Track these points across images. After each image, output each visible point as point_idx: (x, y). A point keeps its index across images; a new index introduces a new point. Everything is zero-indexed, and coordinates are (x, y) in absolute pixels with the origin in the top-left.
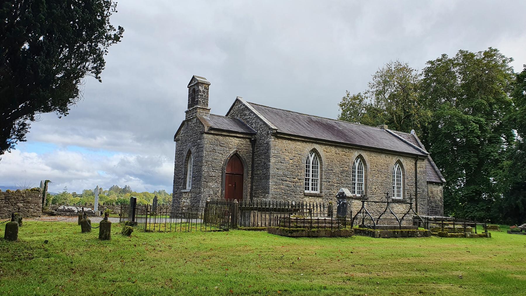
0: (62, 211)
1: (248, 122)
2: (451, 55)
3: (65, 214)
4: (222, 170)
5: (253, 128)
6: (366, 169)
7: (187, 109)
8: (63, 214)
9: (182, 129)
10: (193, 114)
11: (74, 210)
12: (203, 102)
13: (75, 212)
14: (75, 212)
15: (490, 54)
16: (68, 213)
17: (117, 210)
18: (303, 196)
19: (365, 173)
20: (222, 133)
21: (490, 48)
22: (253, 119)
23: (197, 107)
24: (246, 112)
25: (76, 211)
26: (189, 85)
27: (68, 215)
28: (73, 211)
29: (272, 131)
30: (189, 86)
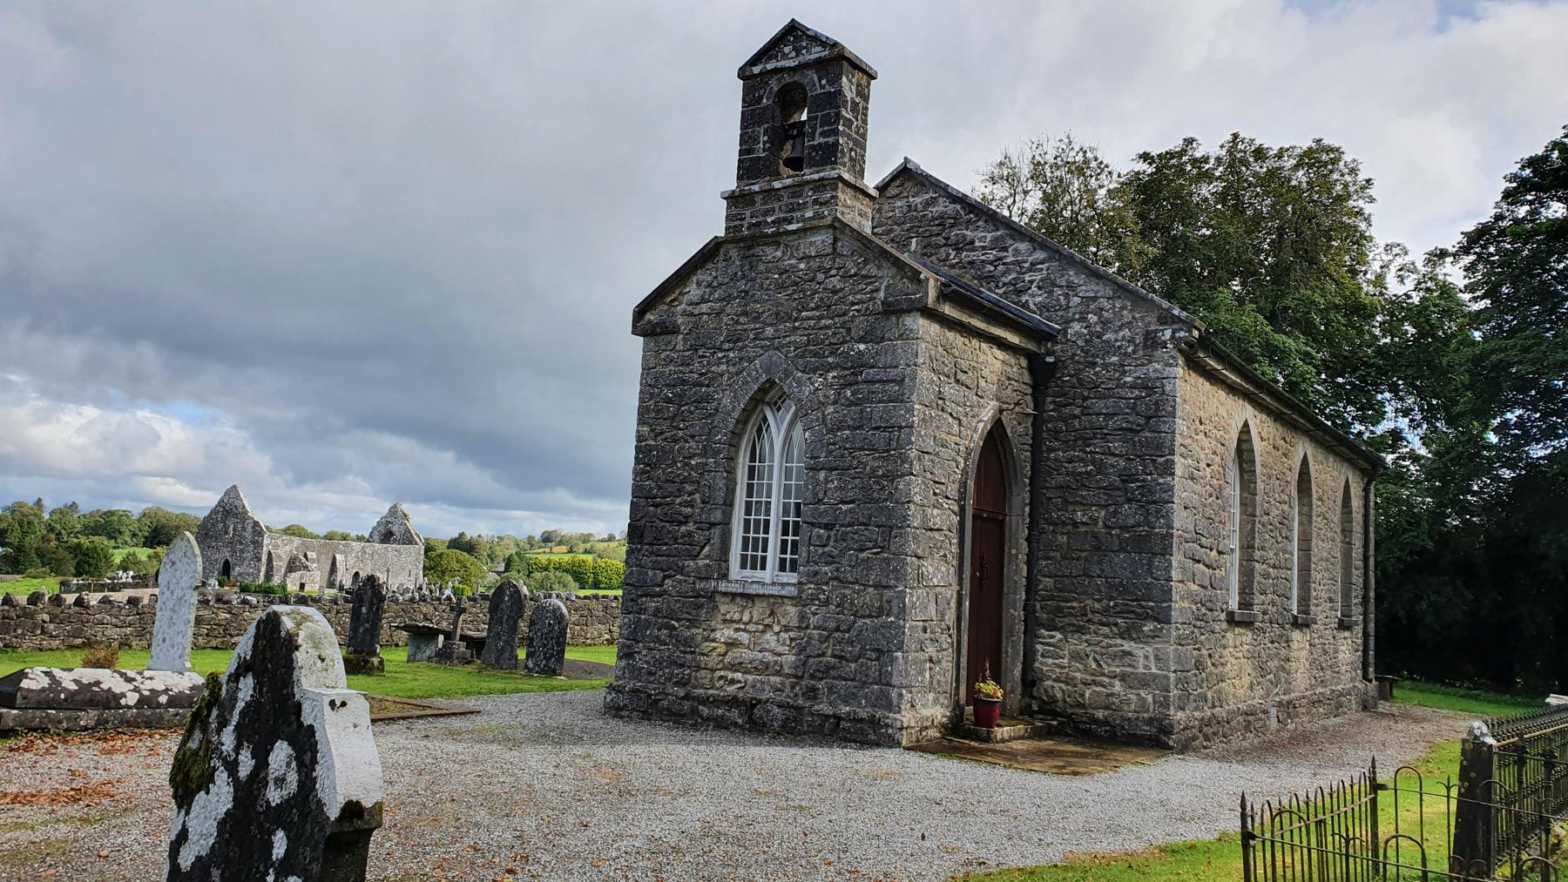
0: (49, 699)
1: (990, 278)
2: (1211, 146)
3: (68, 719)
4: (960, 500)
5: (1028, 309)
6: (1306, 509)
7: (732, 184)
8: (60, 722)
9: (701, 276)
10: (791, 211)
11: (117, 691)
12: (851, 159)
13: (123, 702)
14: (129, 707)
15: (1319, 158)
16: (87, 717)
17: (99, 628)
18: (1224, 625)
19: (1300, 524)
20: (971, 317)
21: (1320, 140)
22: (1026, 265)
23: (840, 178)
24: (968, 233)
25: (132, 699)
26: (754, 61)
27: (85, 729)
28: (111, 700)
29: (1182, 334)
30: (756, 70)
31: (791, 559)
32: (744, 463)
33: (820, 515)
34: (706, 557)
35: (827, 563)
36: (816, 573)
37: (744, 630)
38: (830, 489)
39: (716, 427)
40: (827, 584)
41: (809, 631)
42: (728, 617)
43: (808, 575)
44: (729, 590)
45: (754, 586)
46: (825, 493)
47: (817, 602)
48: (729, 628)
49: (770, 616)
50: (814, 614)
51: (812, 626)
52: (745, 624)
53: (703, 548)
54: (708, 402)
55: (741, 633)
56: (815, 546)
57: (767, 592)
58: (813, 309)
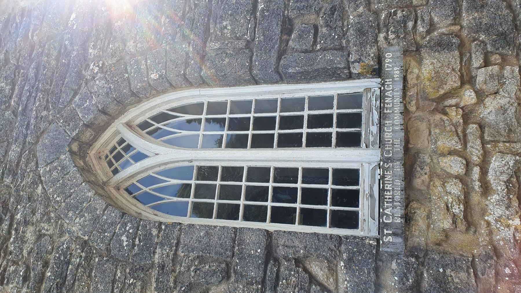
31: (274, 200)
32: (278, 93)
33: (268, 39)
34: (332, 270)
35: (343, 17)
36: (360, 32)
37: (484, 172)
38: (233, 31)
39: (108, 250)
40: (377, 13)
41: (465, 33)
42: (458, 209)
43: (362, 45)
44: (398, 196)
45: (388, 135)
46: (238, 39)
47: (410, 24)
48: (484, 212)
49: (446, 114)
50: (432, 27)
51: (457, 28)
52: (468, 165)
53: (312, 279)
54: (68, 263)
55: (491, 176)
56: (315, 43)
57: (398, 108)
58: (13, 89)
